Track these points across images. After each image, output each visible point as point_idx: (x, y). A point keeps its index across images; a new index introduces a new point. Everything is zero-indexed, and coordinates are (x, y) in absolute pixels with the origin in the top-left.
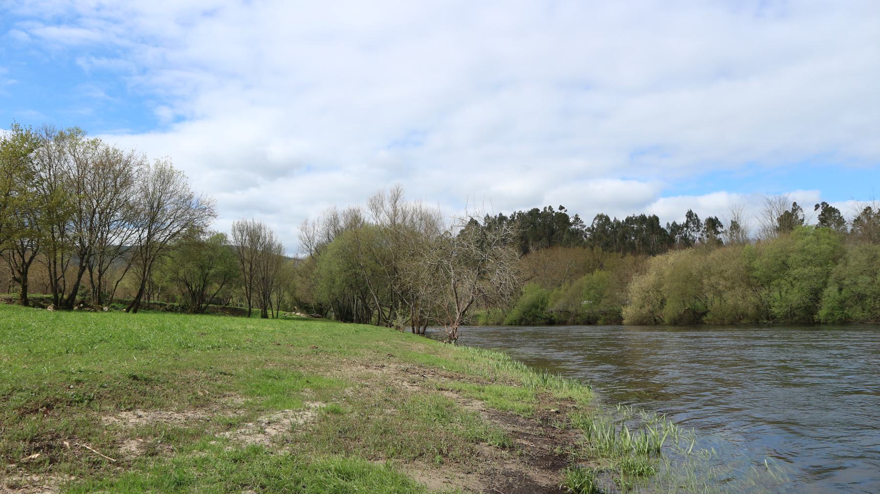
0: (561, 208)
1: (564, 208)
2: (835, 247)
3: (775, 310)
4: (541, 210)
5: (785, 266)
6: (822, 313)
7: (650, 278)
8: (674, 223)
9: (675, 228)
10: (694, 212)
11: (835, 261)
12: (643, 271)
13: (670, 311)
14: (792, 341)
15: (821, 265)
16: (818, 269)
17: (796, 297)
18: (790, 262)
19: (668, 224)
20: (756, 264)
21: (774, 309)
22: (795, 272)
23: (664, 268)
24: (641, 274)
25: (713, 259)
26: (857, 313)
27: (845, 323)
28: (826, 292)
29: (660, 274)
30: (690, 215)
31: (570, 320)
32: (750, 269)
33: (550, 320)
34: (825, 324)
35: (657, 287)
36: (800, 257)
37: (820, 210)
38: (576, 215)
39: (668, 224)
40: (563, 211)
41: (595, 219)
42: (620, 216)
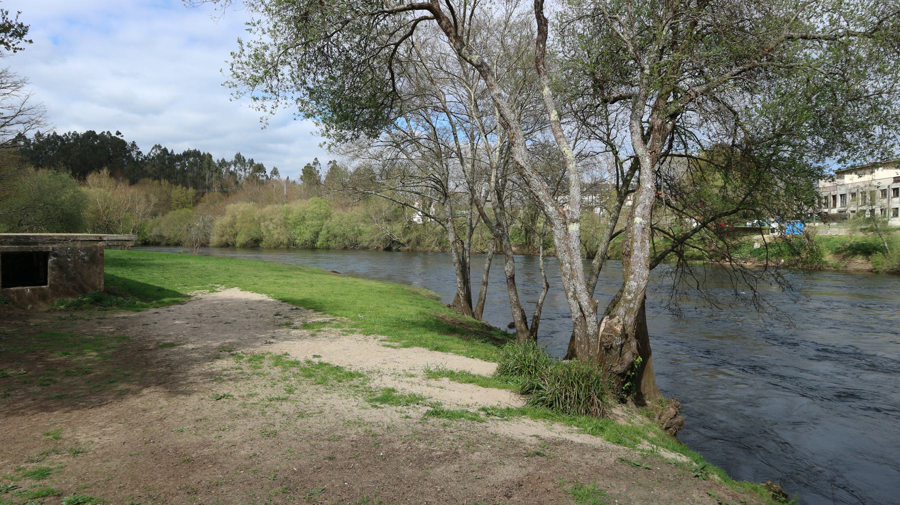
0: (118, 133)
1: (120, 134)
2: (327, 210)
3: (297, 241)
4: (98, 133)
5: (304, 219)
6: (318, 244)
7: (227, 219)
8: (223, 160)
9: (223, 163)
10: (242, 154)
11: (326, 218)
12: (223, 213)
13: (241, 239)
14: (866, 343)
15: (320, 220)
16: (319, 222)
17: (308, 235)
18: (306, 217)
19: (218, 161)
20: (290, 216)
21: (297, 241)
22: (307, 223)
23: (236, 213)
24: (221, 216)
25: (267, 211)
26: (333, 244)
27: (328, 249)
28: (321, 233)
29: (234, 217)
30: (238, 157)
31: (164, 243)
32: (286, 218)
33: (145, 241)
34: (319, 249)
35: (232, 225)
36: (311, 215)
37: (331, 165)
38: (134, 142)
39: (218, 161)
40: (119, 137)
41: (153, 149)
42: (178, 149)
